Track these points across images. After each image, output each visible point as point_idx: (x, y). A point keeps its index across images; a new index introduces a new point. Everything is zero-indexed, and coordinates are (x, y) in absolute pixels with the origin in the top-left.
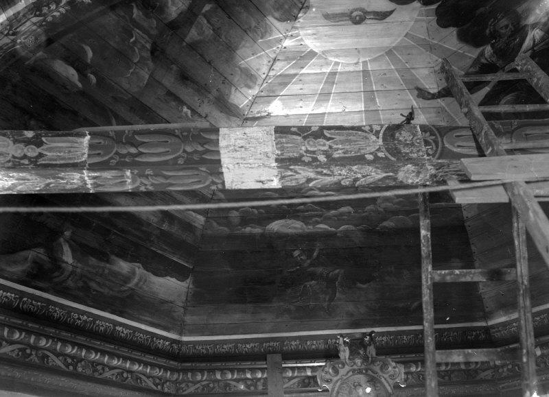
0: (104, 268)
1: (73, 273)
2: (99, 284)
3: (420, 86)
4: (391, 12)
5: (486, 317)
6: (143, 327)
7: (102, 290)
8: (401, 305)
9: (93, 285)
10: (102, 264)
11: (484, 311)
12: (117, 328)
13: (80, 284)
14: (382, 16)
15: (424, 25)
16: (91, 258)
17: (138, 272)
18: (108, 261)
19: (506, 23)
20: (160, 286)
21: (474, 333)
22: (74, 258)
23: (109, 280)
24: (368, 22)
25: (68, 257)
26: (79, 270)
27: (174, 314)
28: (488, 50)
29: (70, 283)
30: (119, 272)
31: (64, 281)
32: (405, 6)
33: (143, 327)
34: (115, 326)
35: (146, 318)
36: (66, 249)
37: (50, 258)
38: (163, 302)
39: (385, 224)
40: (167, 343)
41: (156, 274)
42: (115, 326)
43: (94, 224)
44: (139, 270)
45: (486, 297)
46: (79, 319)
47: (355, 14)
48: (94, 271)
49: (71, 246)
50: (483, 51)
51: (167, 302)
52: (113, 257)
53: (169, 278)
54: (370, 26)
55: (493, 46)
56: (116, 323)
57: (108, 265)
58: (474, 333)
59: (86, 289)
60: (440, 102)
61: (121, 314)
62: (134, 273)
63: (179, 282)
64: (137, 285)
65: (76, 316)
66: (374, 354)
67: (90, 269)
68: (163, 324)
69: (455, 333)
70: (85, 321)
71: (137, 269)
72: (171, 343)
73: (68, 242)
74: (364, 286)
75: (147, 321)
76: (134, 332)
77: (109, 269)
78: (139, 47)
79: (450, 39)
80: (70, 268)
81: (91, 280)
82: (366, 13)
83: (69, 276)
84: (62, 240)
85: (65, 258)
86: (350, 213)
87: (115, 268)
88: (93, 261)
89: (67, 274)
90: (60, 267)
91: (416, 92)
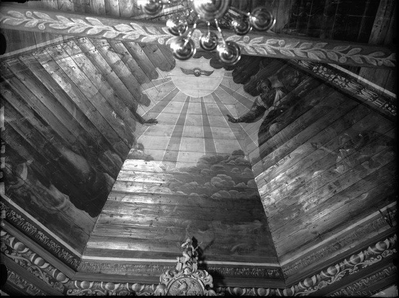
0: (45, 191)
1: (23, 186)
2: (37, 199)
3: (229, 114)
4: (212, 72)
5: (278, 261)
6: (57, 238)
7: (38, 204)
8: (225, 247)
9: (33, 198)
10: (44, 188)
11: (277, 256)
12: (39, 232)
13: (25, 195)
14: (208, 74)
15: (227, 80)
16: (38, 181)
17: (65, 201)
18: (48, 187)
19: (265, 85)
20: (77, 215)
21: (272, 271)
22: (28, 178)
23: (45, 200)
24: (202, 76)
25: (24, 175)
26: (28, 186)
27: (82, 238)
28: (259, 98)
29: (19, 192)
30: (53, 197)
31: (16, 189)
32: (218, 70)
33: (57, 238)
34: (38, 230)
35: (61, 234)
36: (25, 170)
37: (12, 172)
38: (76, 227)
39: (216, 194)
40: (71, 257)
41: (78, 206)
42: (38, 230)
43: (48, 163)
44: (67, 200)
45: (277, 246)
46: (15, 216)
47: (196, 71)
48: (37, 190)
49: (28, 170)
50: (257, 99)
51: (79, 227)
52: (52, 186)
53: (84, 211)
54: (203, 79)
55: (261, 96)
56: (39, 229)
57: (47, 190)
58: (272, 271)
59: (28, 199)
60: (241, 125)
61: (45, 224)
62: (62, 201)
63: (91, 218)
64: (62, 209)
65: (14, 213)
66: (196, 268)
67: (35, 188)
68: (72, 241)
69: (260, 270)
70: (19, 220)
71: (65, 198)
72: (74, 258)
73: (27, 166)
74: (203, 233)
75: (61, 235)
76: (50, 240)
77: (48, 193)
78: (163, 207)
79: (240, 90)
80: (23, 183)
81: (33, 195)
82: (201, 71)
83: (20, 187)
84: (24, 164)
85: (22, 176)
86: (196, 185)
87: (51, 193)
88: (39, 183)
89: (19, 185)
90: (16, 180)
91: (228, 118)
